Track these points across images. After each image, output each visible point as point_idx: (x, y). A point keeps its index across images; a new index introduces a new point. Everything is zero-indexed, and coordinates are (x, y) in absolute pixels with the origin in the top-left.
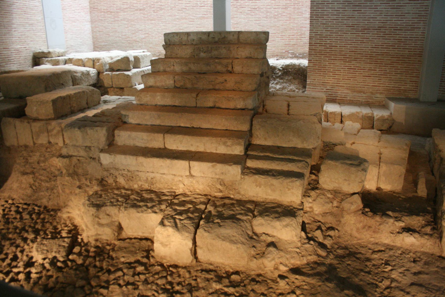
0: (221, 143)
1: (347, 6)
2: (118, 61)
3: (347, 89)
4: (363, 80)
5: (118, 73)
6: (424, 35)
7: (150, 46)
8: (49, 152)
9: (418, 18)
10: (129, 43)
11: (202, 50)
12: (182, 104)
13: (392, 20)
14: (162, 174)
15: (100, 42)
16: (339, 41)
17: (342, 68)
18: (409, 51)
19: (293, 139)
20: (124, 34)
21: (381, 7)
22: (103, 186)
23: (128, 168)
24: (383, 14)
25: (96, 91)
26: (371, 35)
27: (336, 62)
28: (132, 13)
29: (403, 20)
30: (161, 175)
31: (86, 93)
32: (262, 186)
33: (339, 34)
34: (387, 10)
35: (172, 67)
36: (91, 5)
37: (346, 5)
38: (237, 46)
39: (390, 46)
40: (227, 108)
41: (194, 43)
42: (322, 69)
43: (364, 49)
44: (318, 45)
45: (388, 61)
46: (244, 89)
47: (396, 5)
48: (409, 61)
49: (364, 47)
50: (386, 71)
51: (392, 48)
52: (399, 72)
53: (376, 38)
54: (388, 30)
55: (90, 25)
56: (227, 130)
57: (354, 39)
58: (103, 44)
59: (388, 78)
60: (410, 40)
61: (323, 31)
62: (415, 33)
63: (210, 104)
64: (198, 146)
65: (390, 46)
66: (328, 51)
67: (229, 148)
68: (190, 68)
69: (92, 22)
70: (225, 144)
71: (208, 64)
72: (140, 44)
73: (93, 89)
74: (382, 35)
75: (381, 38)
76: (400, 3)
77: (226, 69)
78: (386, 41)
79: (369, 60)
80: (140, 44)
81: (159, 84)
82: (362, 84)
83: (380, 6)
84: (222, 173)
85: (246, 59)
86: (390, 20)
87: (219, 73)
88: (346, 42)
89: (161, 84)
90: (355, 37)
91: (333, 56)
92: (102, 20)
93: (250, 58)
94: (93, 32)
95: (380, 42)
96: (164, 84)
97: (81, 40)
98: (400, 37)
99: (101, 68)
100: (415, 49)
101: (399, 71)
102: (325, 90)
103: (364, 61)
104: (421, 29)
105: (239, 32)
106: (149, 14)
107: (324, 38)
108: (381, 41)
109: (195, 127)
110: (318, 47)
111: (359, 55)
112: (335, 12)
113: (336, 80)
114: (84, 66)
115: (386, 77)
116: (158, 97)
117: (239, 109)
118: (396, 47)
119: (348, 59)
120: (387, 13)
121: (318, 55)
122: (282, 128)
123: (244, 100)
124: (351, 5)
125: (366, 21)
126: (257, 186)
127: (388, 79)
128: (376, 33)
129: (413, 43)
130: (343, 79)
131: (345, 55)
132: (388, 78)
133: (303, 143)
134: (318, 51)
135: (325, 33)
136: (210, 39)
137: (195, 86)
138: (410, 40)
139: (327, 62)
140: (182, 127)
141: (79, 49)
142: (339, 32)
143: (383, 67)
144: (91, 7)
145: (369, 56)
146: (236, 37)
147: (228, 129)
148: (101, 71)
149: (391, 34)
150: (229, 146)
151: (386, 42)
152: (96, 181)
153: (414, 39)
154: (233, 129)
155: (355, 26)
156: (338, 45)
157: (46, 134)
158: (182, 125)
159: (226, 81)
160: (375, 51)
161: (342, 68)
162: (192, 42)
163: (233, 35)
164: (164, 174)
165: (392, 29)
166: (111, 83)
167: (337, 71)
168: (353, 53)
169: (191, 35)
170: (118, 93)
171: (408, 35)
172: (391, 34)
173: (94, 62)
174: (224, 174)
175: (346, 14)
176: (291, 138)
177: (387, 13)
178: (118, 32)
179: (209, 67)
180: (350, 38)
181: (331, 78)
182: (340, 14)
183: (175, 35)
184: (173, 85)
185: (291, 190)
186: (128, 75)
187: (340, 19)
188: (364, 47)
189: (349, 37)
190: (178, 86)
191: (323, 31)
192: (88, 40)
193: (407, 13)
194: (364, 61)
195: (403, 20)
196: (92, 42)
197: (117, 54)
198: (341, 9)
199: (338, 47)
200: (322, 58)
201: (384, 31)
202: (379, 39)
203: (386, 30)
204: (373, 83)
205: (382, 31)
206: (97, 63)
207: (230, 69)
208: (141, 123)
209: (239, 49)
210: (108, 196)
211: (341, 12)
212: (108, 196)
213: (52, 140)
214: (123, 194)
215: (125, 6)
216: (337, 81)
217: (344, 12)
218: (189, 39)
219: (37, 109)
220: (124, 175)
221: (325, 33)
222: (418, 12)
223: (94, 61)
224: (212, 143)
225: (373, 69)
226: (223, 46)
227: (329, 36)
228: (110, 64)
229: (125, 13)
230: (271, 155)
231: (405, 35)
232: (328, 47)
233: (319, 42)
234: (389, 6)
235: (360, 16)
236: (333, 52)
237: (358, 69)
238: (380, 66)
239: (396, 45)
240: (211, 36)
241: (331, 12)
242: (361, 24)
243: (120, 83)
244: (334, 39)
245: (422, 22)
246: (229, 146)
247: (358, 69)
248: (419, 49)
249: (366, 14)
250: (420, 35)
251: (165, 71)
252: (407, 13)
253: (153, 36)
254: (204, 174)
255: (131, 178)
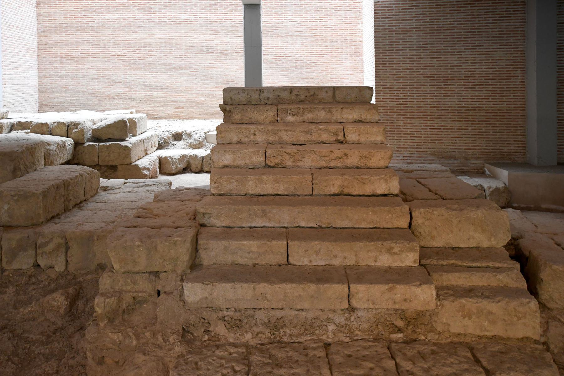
0: (383, 250)
1: (422, 52)
2: (109, 126)
3: (432, 154)
4: (452, 143)
5: (108, 144)
6: (524, 85)
7: (132, 104)
8: (33, 284)
9: (513, 65)
10: (99, 100)
11: (289, 112)
12: (291, 190)
13: (482, 68)
14: (298, 310)
15: (50, 98)
16: (415, 95)
17: (423, 129)
18: (507, 104)
19: (475, 236)
20: (91, 87)
21: (466, 53)
22: (189, 343)
23: (235, 305)
24: (469, 62)
25: (95, 173)
26: (456, 86)
27: (413, 121)
28: (106, 59)
29: (495, 68)
30: (296, 313)
31: (84, 176)
32: (474, 317)
33: (415, 86)
34: (473, 56)
35: (252, 137)
36: (40, 46)
37: (422, 51)
38: (342, 106)
39: (482, 99)
40: (361, 194)
41: (270, 102)
42: (396, 130)
43: (450, 103)
44: (388, 100)
45: (482, 117)
46: (373, 165)
47: (484, 50)
48: (509, 116)
49: (449, 102)
50: (481, 129)
51: (486, 102)
52: (498, 131)
53: (463, 89)
54: (477, 79)
55: (37, 74)
56: (375, 228)
57: (436, 92)
58: (56, 100)
59: (484, 138)
60: (507, 91)
61: (393, 83)
62: (513, 82)
63: (334, 190)
64: (345, 258)
65: (482, 99)
66: (402, 108)
67: (396, 256)
68: (280, 138)
69: (40, 69)
70: (389, 251)
71: (308, 132)
72: (116, 102)
73: (93, 171)
74: (470, 86)
75: (470, 89)
76: (489, 48)
77: (334, 138)
78: (477, 93)
79: (456, 117)
80: (116, 102)
81: (239, 162)
82: (452, 147)
83: (464, 52)
84: (405, 300)
85: (355, 123)
86: (479, 68)
87: (324, 143)
88: (425, 96)
89: (243, 162)
90: (436, 89)
91: (408, 114)
92: (56, 68)
93: (361, 121)
94: (40, 83)
95: (470, 95)
96: (248, 162)
97: (23, 95)
98: (494, 88)
99: (81, 137)
100: (515, 101)
101: (498, 128)
102: (401, 158)
103: (451, 118)
104: (519, 78)
105: (334, 88)
106: (132, 61)
107: (395, 92)
108: (470, 93)
109: (324, 226)
110: (388, 102)
111: (443, 111)
112: (408, 60)
113: (416, 144)
114: (51, 134)
115: (482, 138)
116: (251, 183)
117: (378, 196)
118: (490, 100)
119: (429, 117)
120: (474, 60)
121: (388, 113)
122: (458, 219)
123: (386, 181)
124: (428, 51)
125: (449, 71)
126: (464, 317)
127: (485, 139)
128: (462, 83)
129: (512, 95)
130: (424, 143)
131: (425, 112)
132: (484, 138)
133: (489, 240)
134: (388, 108)
135: (396, 85)
136: (293, 97)
137: (299, 164)
138: (507, 91)
139: (402, 122)
140: (303, 227)
141: (19, 108)
142: (415, 84)
143: (477, 125)
144: (39, 50)
145: (457, 112)
146: (330, 93)
147: (378, 226)
148: (80, 142)
149: (483, 85)
150: (396, 254)
151: (477, 95)
152: (175, 336)
153: (512, 89)
154: (385, 226)
155: (435, 76)
156: (415, 100)
157: (31, 252)
158: (303, 224)
159: (346, 155)
160: (464, 105)
161: (423, 129)
162: (267, 101)
163: (327, 92)
164: (302, 310)
165: (483, 78)
166: (96, 159)
167: (416, 133)
168: (436, 109)
169: (265, 91)
170: (106, 174)
171: (504, 85)
172: (483, 85)
173: (68, 129)
174: (408, 301)
175: (421, 62)
176: (471, 234)
177: (474, 60)
178: (82, 85)
179: (309, 136)
180: (430, 91)
181: (409, 141)
182: (415, 62)
183: (241, 92)
184: (263, 164)
185: (523, 320)
186: (127, 147)
187: (415, 68)
188: (449, 102)
189: (428, 90)
190: (272, 165)
191: (393, 83)
192: (32, 95)
193: (499, 60)
194: (451, 118)
195: (495, 68)
196: (37, 98)
197: (111, 116)
198: (415, 57)
199: (415, 103)
200: (395, 116)
201: (473, 81)
202: (468, 91)
203: (475, 79)
204: (466, 146)
205: (470, 81)
206: (73, 129)
207: (341, 138)
208: (232, 225)
209: (344, 110)
210: (210, 364)
211: (415, 59)
212: (210, 364)
213: (42, 262)
214: (234, 355)
215: (96, 50)
216: (417, 145)
217: (420, 60)
218: (261, 97)
219: (9, 209)
220: (226, 318)
221: (396, 85)
222: (512, 58)
223: (68, 126)
224: (368, 251)
225: (463, 128)
226: (321, 106)
227: (401, 90)
228: (94, 131)
229: (96, 59)
230: (459, 263)
231: (500, 85)
232: (402, 103)
233: (388, 97)
234: (476, 52)
235: (440, 64)
236: (409, 108)
237: (444, 129)
238: (472, 124)
239: (491, 98)
240: (295, 93)
241: (402, 59)
242: (443, 73)
243: (113, 159)
244: (409, 92)
245: (519, 69)
246: (396, 254)
247: (444, 129)
248: (520, 101)
249: (448, 62)
250: (519, 85)
251: (240, 143)
252: (499, 60)
253: (136, 91)
254: (373, 304)
255: (237, 322)
